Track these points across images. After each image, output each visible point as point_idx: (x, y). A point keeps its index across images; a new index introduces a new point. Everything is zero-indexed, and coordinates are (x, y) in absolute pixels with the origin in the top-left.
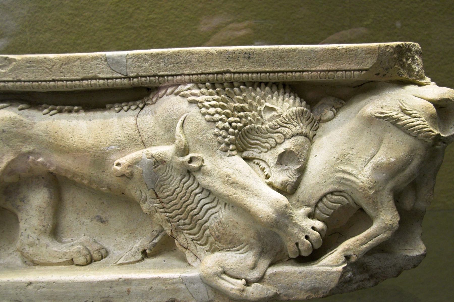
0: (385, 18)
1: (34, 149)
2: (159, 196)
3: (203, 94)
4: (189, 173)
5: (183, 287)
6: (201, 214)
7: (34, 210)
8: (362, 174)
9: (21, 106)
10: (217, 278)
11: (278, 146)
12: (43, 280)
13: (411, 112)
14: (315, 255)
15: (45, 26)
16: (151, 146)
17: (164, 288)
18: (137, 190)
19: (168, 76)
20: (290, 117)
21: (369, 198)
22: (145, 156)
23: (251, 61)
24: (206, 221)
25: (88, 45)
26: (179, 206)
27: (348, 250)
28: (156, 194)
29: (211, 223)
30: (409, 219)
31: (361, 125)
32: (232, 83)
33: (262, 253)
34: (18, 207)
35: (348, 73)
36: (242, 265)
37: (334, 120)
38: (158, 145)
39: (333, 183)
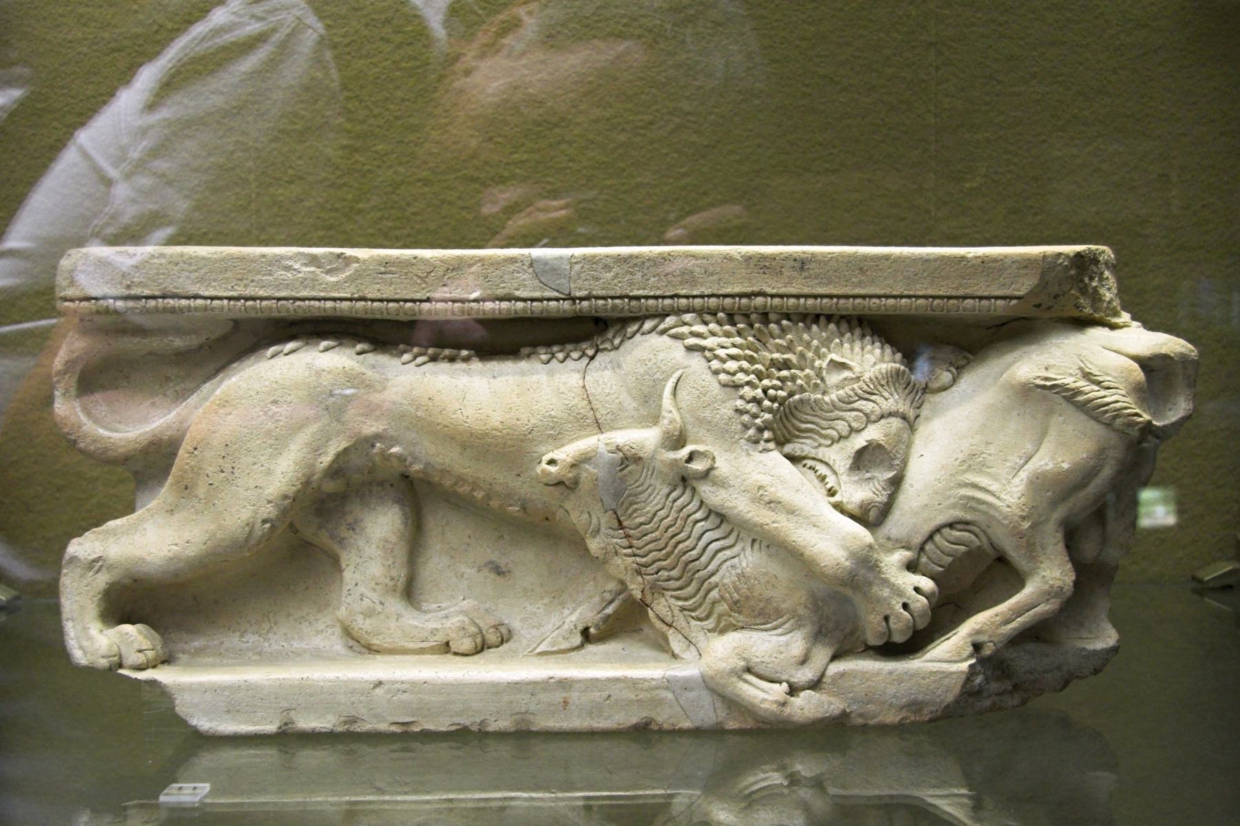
0: (1009, 176)
1: (385, 430)
2: (625, 524)
3: (713, 334)
4: (685, 481)
5: (670, 696)
6: (703, 559)
7: (374, 546)
8: (1007, 493)
9: (359, 347)
10: (735, 679)
11: (853, 435)
12: (404, 678)
13: (1101, 379)
14: (916, 643)
15: (291, 172)
16: (612, 429)
17: (633, 697)
18: (582, 512)
19: (647, 297)
20: (876, 381)
21: (1021, 535)
22: (602, 449)
23: (805, 274)
24: (713, 574)
25: (379, 214)
26: (661, 543)
27: (978, 632)
28: (620, 522)
29: (723, 577)
30: (1091, 577)
31: (1006, 401)
32: (765, 315)
33: (819, 635)
34: (341, 541)
35: (984, 302)
36: (782, 656)
37: (954, 389)
38: (626, 428)
39: (954, 506)
